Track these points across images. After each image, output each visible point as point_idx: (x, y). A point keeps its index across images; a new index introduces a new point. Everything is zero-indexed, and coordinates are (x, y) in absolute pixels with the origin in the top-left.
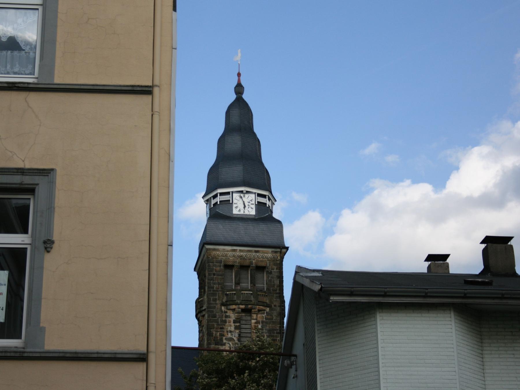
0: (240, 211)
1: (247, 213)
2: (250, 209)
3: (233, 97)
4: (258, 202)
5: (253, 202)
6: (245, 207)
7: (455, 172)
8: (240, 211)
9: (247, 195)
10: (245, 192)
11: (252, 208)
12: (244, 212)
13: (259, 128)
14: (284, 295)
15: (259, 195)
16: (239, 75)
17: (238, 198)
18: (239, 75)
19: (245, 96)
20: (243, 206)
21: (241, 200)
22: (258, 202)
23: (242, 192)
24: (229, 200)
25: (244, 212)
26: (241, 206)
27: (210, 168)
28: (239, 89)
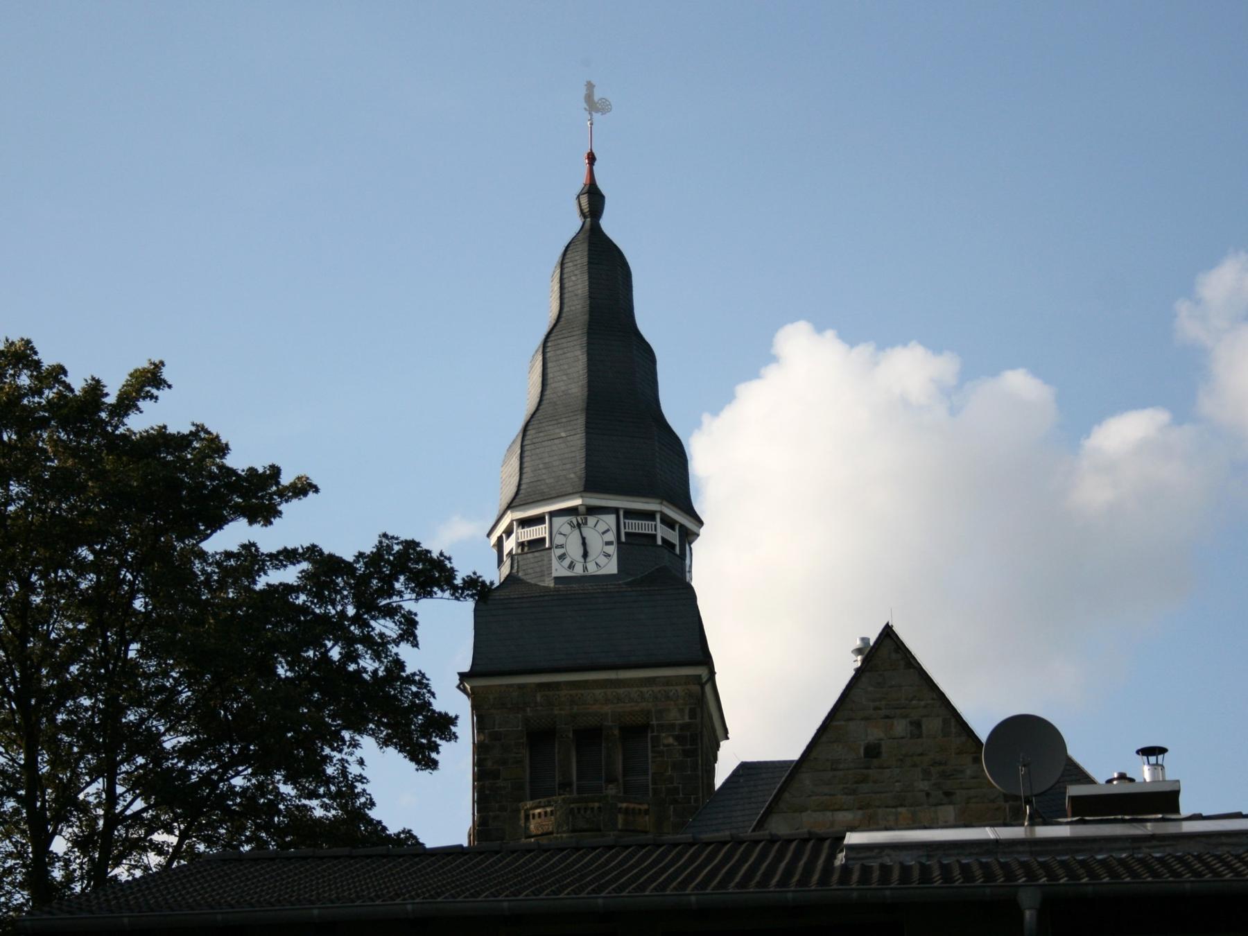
0: (571, 566)
1: (592, 569)
2: (602, 560)
3: (573, 223)
4: (627, 534)
5: (611, 537)
6: (585, 555)
7: (321, 552)
8: (571, 566)
9: (591, 520)
10: (582, 510)
11: (607, 555)
12: (585, 568)
13: (650, 319)
14: (720, 753)
15: (630, 514)
16: (592, 158)
17: (566, 529)
18: (592, 158)
19: (608, 224)
20: (581, 552)
21: (577, 532)
22: (627, 534)
23: (572, 511)
24: (543, 539)
25: (585, 568)
26: (575, 551)
27: (285, 581)
28: (593, 200)
